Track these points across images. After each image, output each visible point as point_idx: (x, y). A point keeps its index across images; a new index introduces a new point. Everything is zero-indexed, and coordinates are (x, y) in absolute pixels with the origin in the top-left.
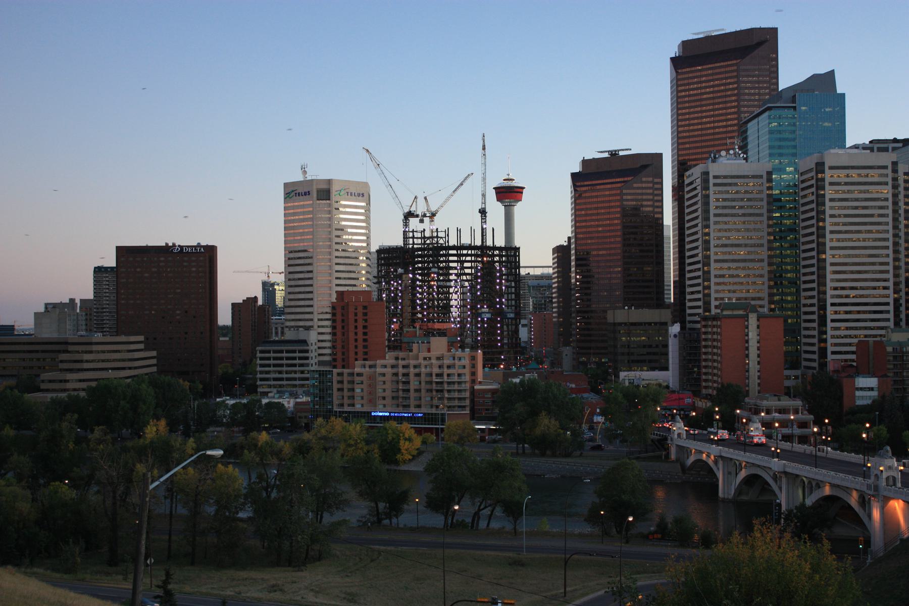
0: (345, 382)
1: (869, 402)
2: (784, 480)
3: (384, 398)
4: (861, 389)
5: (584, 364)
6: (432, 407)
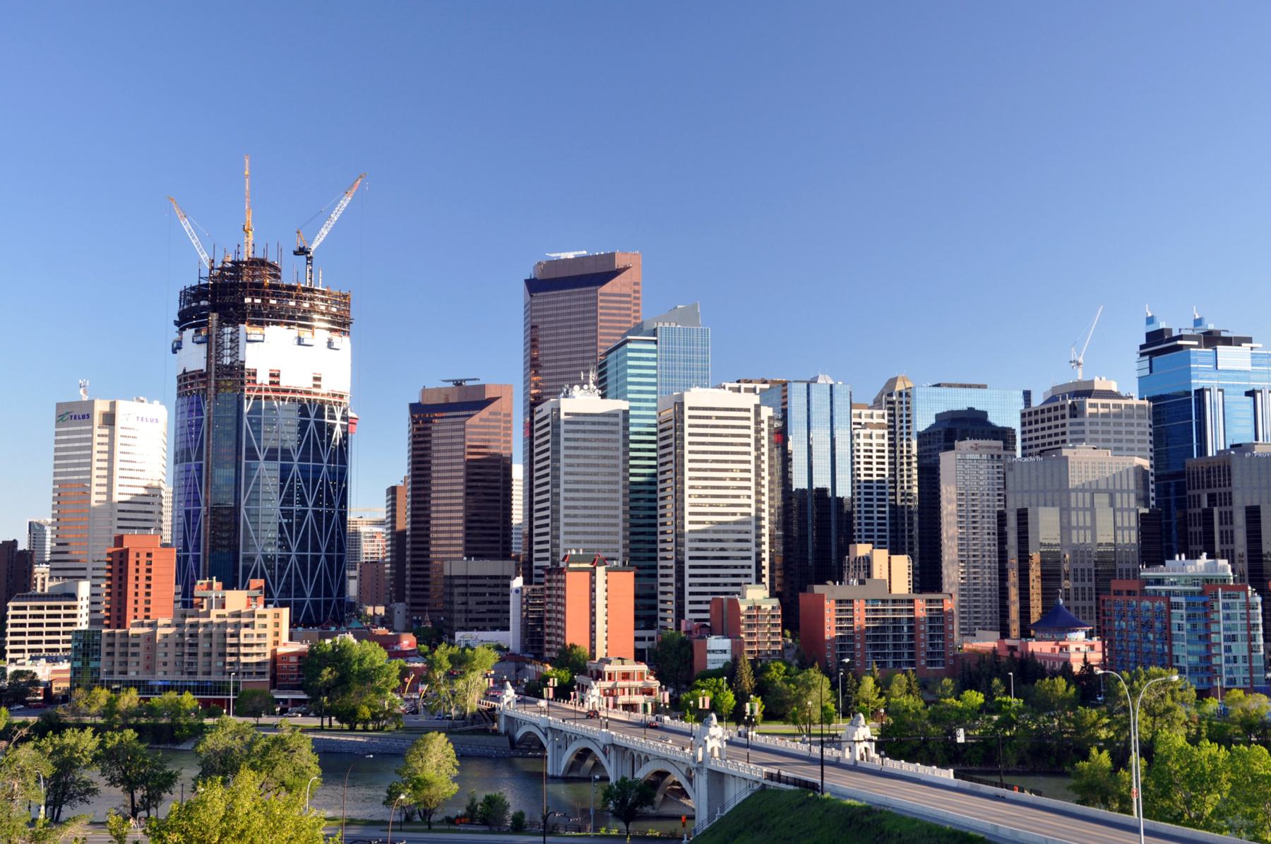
0: (117, 645)
1: (721, 665)
2: (613, 753)
3: (165, 664)
4: (713, 651)
5: (419, 622)
6: (224, 673)
